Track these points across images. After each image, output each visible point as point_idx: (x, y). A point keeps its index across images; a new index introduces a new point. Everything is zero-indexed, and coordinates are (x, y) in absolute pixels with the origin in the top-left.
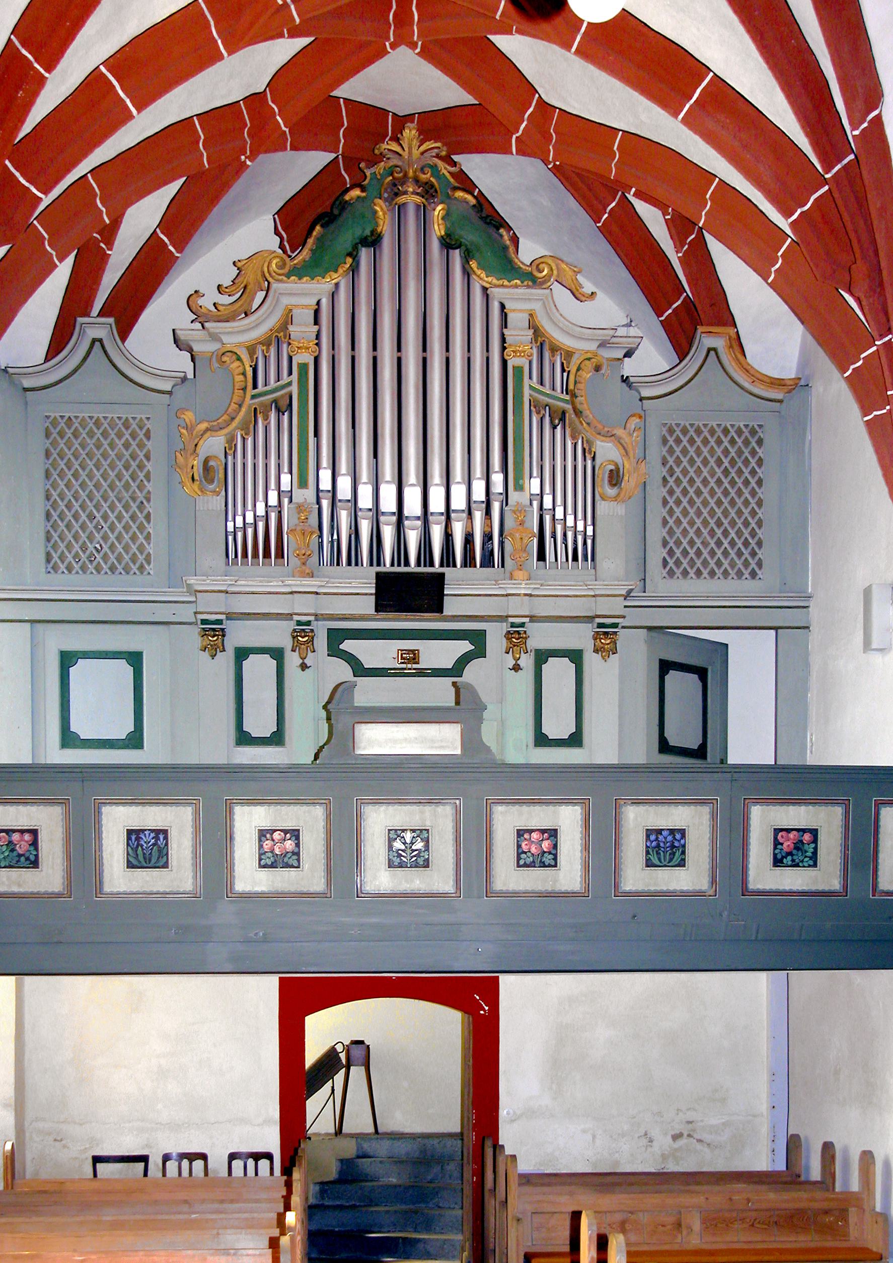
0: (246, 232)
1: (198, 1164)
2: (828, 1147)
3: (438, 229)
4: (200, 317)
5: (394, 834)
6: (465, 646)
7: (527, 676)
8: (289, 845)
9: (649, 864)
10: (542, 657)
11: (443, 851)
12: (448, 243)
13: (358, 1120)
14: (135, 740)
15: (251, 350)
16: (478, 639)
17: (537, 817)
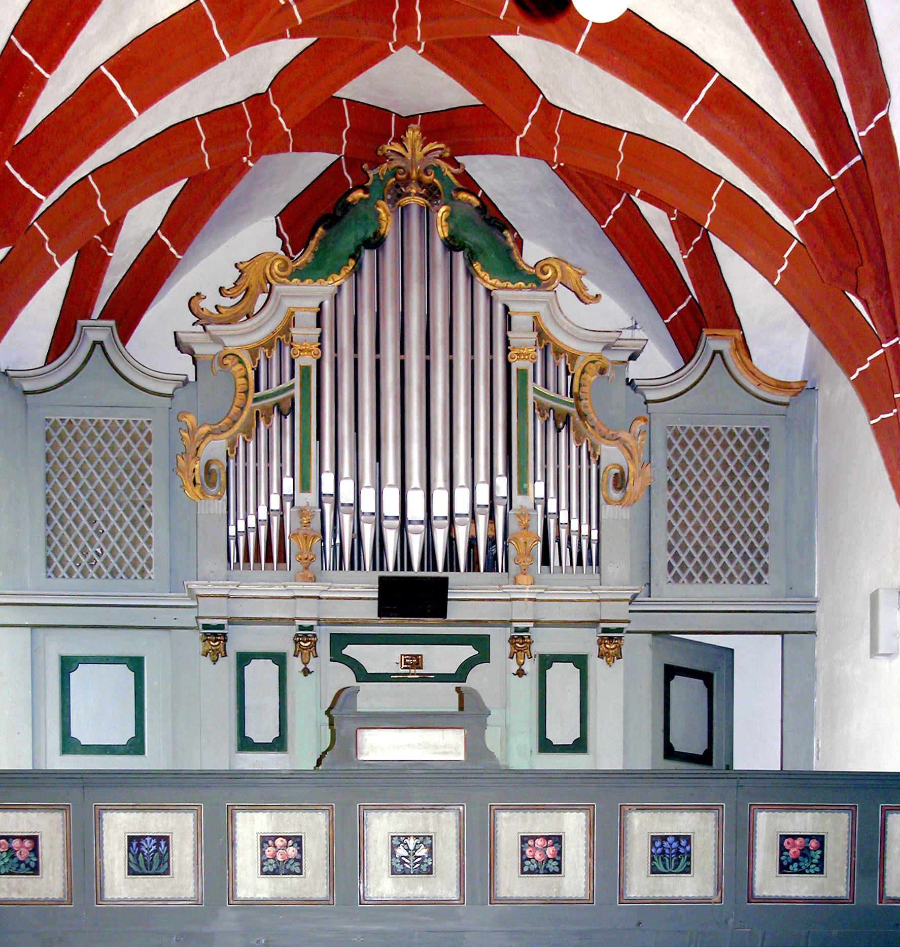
3: (441, 231)
4: (202, 320)
5: (397, 840)
6: (469, 651)
7: (531, 681)
8: (292, 851)
10: (546, 662)
11: (447, 857)
12: (452, 245)
14: (136, 746)
15: (253, 353)
16: (482, 644)
17: (541, 823)
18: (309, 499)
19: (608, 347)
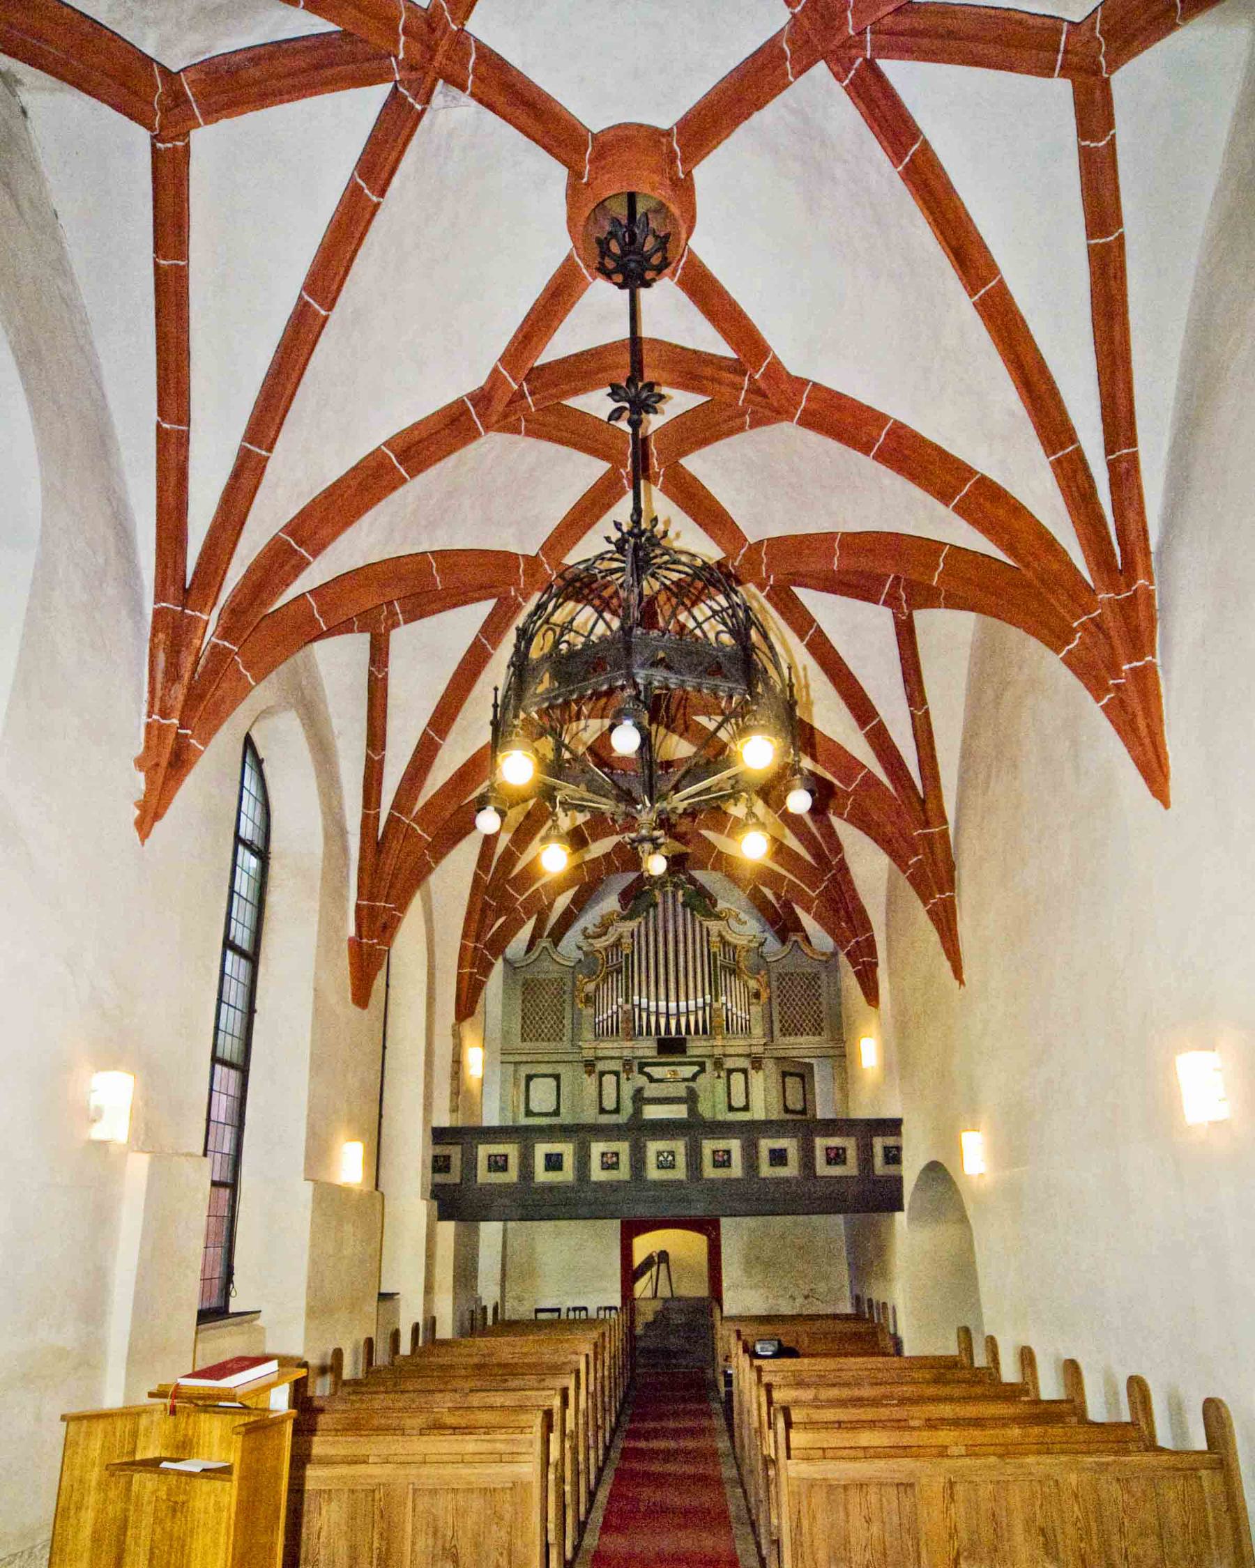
0: (610, 903)
1: (583, 1313)
2: (870, 1300)
3: (681, 899)
4: (587, 937)
5: (659, 1154)
6: (696, 1068)
7: (723, 1081)
8: (614, 1159)
9: (771, 1165)
10: (730, 1072)
11: (681, 1160)
12: (684, 905)
13: (664, 1292)
14: (556, 1113)
15: (606, 949)
16: (702, 1066)
17: (722, 1144)
18: (629, 1006)
19: (750, 941)
